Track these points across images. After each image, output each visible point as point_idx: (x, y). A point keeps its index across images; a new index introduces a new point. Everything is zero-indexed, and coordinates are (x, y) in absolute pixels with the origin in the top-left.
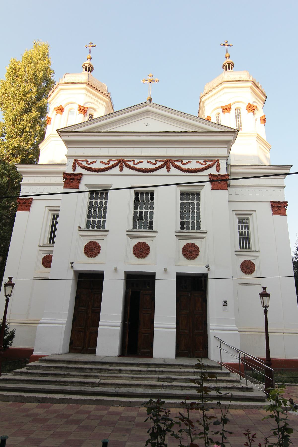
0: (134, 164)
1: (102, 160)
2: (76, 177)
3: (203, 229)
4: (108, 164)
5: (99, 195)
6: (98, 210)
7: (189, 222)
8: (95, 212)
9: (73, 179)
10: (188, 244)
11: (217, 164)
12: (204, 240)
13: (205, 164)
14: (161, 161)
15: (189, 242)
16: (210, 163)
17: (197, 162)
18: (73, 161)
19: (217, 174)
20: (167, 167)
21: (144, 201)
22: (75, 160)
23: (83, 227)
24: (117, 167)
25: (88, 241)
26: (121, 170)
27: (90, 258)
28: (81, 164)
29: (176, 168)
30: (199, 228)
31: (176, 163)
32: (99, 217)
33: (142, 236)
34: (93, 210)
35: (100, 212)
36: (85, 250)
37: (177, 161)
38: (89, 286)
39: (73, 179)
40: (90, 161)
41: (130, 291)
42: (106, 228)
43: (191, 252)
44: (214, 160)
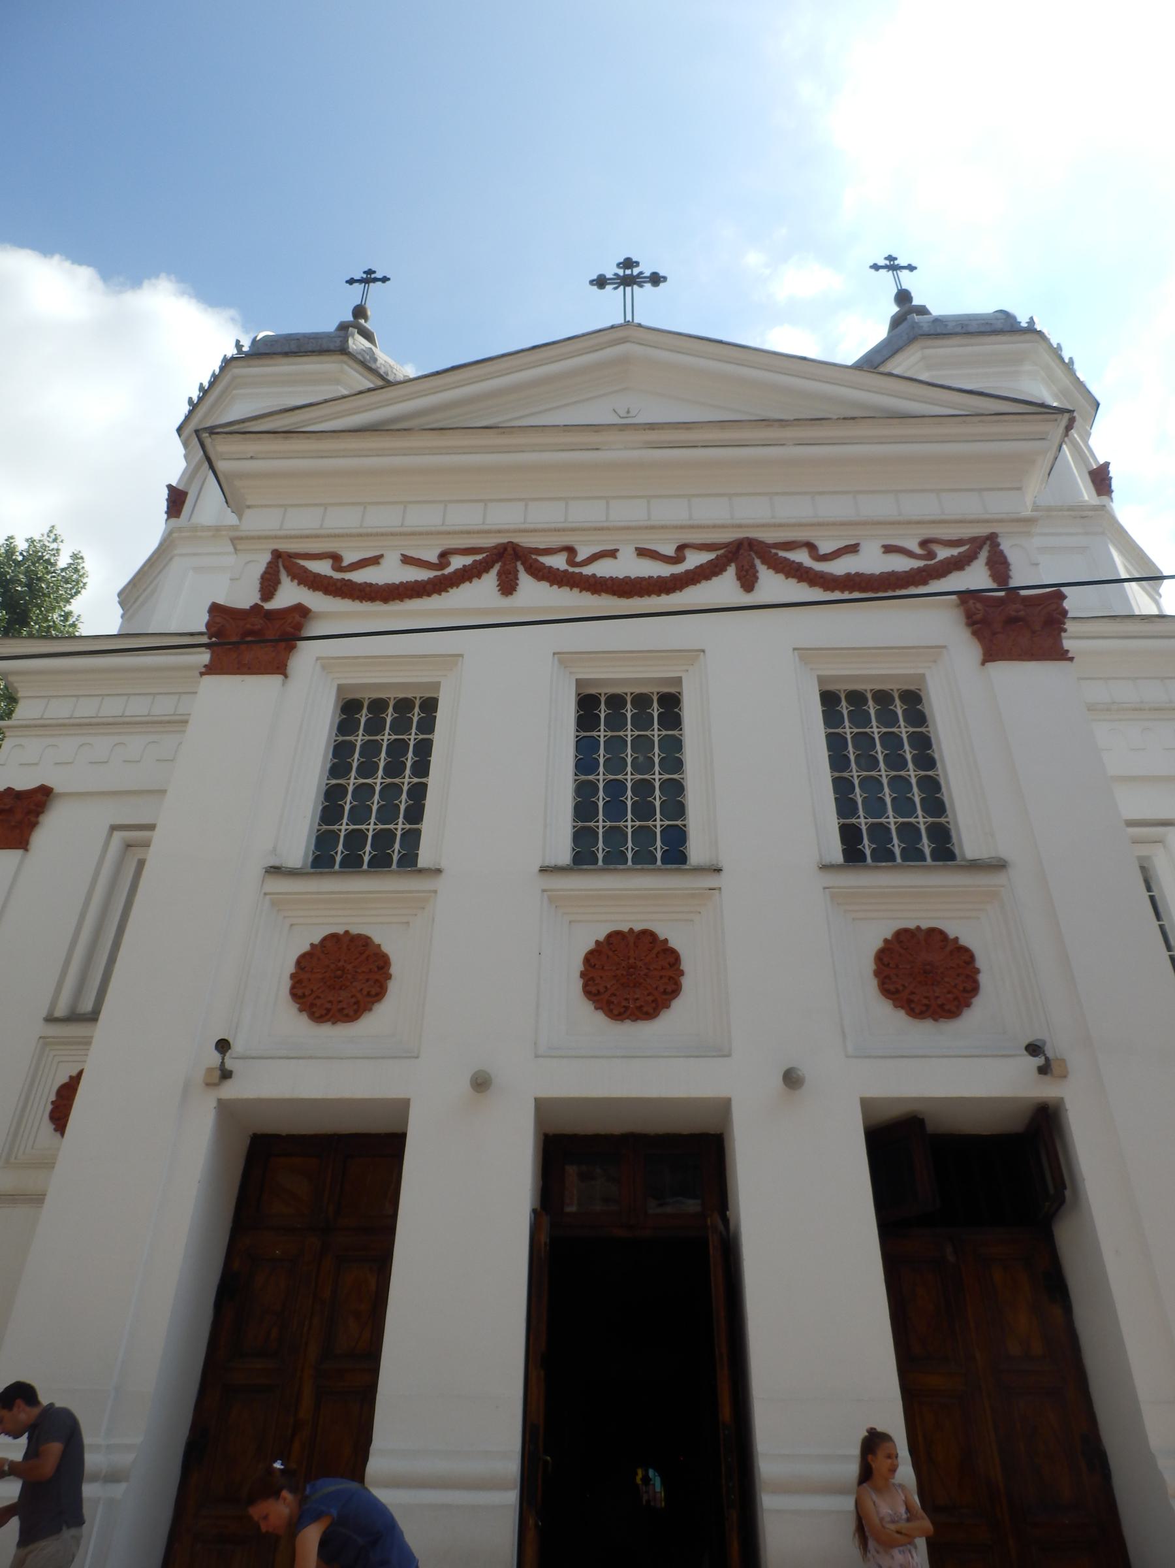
6: (378, 781)
7: (885, 829)
8: (364, 792)
13: (931, 555)
16: (955, 552)
17: (889, 549)
18: (267, 557)
21: (629, 733)
24: (485, 577)
26: (748, 581)
28: (306, 570)
29: (788, 575)
31: (782, 554)
32: (388, 813)
33: (629, 900)
34: (352, 781)
35: (390, 791)
38: (307, 1212)
40: (349, 558)
41: (544, 1238)
44: (973, 540)
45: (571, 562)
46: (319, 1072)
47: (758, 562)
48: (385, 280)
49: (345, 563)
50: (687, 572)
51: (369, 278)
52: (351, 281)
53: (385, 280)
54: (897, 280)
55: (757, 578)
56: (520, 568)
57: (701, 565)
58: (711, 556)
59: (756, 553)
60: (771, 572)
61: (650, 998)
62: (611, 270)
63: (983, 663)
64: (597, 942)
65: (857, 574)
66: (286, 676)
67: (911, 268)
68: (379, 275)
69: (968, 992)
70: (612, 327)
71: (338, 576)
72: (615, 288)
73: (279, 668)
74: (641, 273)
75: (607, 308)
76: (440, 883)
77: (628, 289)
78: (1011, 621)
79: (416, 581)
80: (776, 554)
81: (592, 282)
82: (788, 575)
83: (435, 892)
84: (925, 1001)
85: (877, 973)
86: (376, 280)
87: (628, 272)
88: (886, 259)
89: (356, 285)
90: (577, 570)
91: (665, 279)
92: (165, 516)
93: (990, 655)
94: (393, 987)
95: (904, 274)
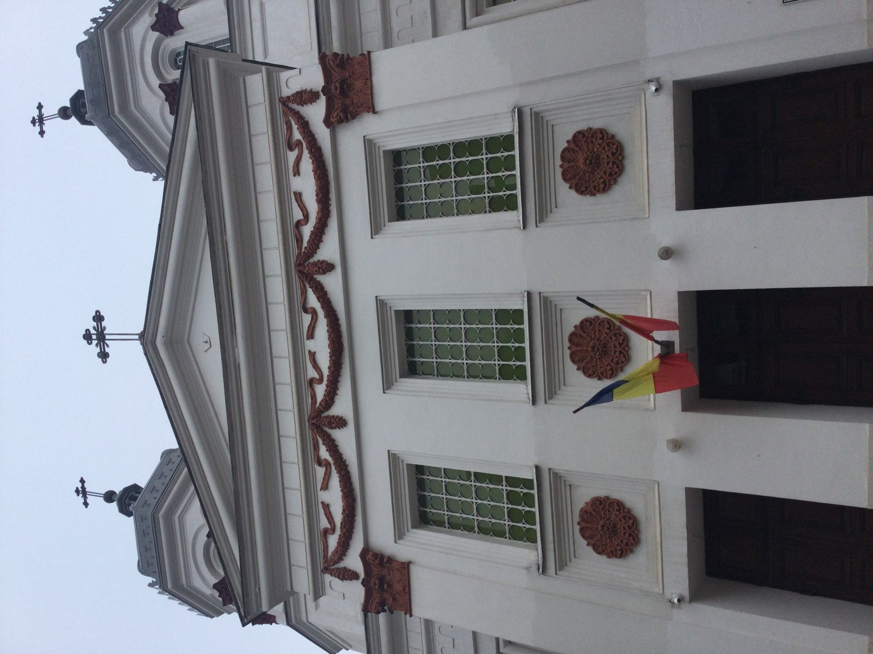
0: (333, 530)
1: (319, 485)
2: (376, 571)
3: (506, 126)
4: (327, 465)
5: (427, 496)
9: (382, 580)
10: (582, 531)
11: (294, 101)
12: (548, 117)
13: (299, 144)
14: (316, 448)
15: (559, 171)
16: (295, 127)
17: (297, 172)
19: (323, 98)
20: (319, 273)
22: (326, 570)
23: (515, 216)
25: (582, 542)
27: (643, 536)
28: (336, 551)
30: (506, 142)
31: (305, 244)
36: (612, 554)
37: (299, 239)
39: (382, 580)
40: (324, 523)
42: (531, 475)
43: (594, 162)
44: (285, 114)
45: (321, 381)
46: (668, 542)
47: (312, 260)
48: (82, 481)
49: (329, 526)
50: (323, 308)
51: (82, 492)
52: (86, 504)
53: (82, 481)
54: (52, 117)
55: (323, 261)
56: (326, 414)
57: (318, 298)
58: (310, 292)
59: (305, 261)
60: (318, 251)
61: (613, 338)
62: (94, 349)
63: (375, 112)
64: (578, 369)
65: (317, 195)
66: (410, 562)
67: (40, 107)
68: (79, 485)
69: (603, 136)
70: (146, 354)
71: (338, 532)
72: (108, 346)
73: (406, 567)
74: (94, 328)
75: (129, 357)
76: (545, 468)
77: (107, 337)
78: (344, 93)
79: (340, 481)
80: (306, 248)
81: (105, 362)
82: (320, 240)
83: (550, 469)
84: (610, 165)
85: (593, 194)
86: (83, 488)
87: (94, 337)
88: (34, 125)
89: (88, 501)
90: (325, 378)
91: (98, 312)
92: (274, 624)
93: (371, 109)
94: (615, 495)
95: (46, 112)
